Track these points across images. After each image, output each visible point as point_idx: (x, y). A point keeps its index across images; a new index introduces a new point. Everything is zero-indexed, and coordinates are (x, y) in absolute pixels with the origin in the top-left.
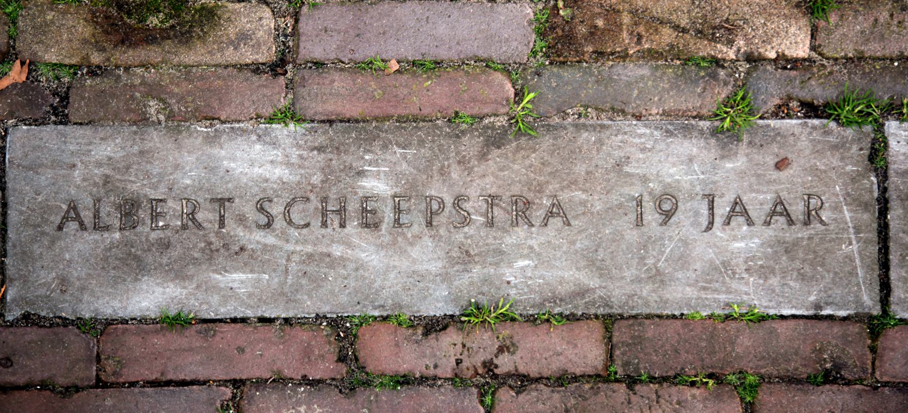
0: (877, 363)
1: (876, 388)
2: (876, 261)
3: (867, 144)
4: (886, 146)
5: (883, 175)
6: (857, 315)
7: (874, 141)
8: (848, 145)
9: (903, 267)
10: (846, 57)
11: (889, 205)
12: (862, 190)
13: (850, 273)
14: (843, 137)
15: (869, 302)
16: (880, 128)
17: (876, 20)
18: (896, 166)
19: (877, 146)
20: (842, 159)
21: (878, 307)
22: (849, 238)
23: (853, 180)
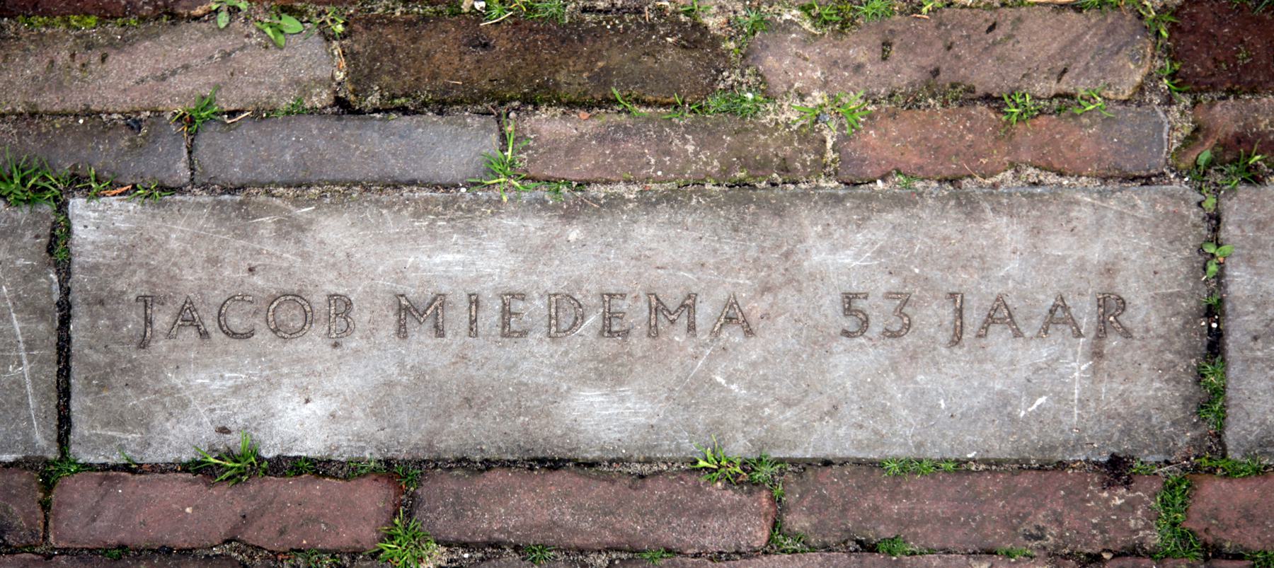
0: (51, 524)
1: (50, 557)
2: (54, 386)
3: (45, 229)
4: (69, 231)
5: (64, 270)
6: (27, 459)
7: (54, 226)
8: (19, 231)
9: (88, 394)
10: (13, 112)
11: (72, 312)
12: (37, 291)
13: (18, 404)
14: (13, 220)
15: (43, 441)
16: (62, 207)
17: (52, 62)
18: (82, 259)
19: (57, 232)
20: (12, 250)
21: (55, 449)
22: (19, 357)
23: (26, 278)
